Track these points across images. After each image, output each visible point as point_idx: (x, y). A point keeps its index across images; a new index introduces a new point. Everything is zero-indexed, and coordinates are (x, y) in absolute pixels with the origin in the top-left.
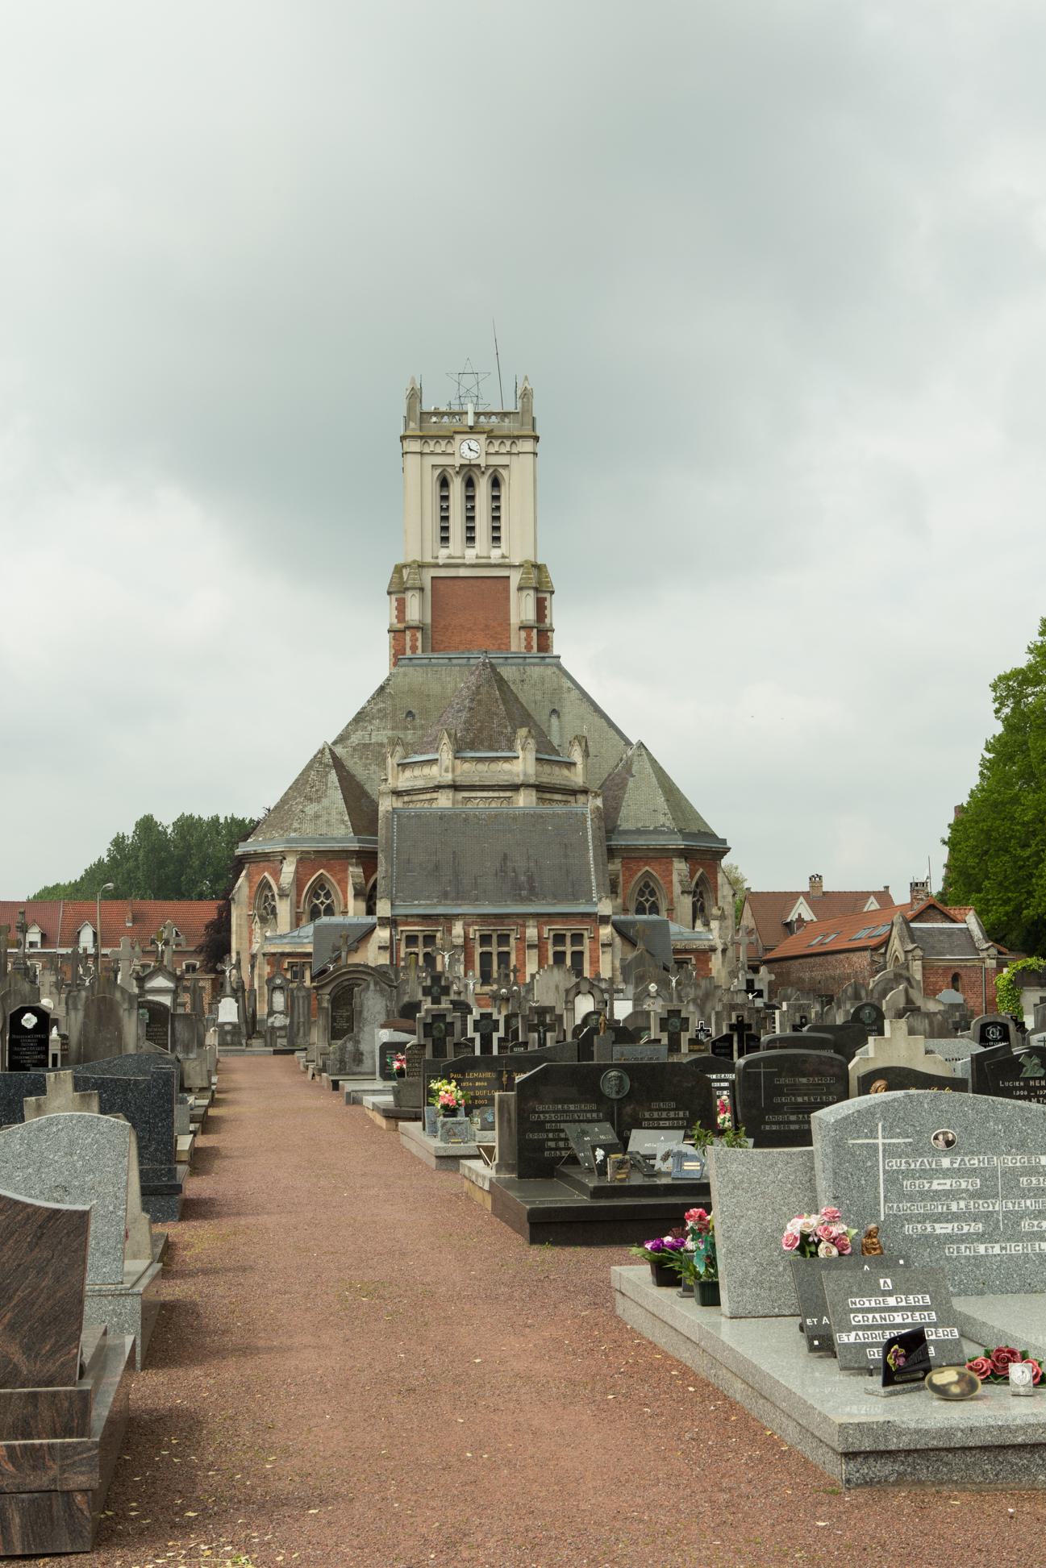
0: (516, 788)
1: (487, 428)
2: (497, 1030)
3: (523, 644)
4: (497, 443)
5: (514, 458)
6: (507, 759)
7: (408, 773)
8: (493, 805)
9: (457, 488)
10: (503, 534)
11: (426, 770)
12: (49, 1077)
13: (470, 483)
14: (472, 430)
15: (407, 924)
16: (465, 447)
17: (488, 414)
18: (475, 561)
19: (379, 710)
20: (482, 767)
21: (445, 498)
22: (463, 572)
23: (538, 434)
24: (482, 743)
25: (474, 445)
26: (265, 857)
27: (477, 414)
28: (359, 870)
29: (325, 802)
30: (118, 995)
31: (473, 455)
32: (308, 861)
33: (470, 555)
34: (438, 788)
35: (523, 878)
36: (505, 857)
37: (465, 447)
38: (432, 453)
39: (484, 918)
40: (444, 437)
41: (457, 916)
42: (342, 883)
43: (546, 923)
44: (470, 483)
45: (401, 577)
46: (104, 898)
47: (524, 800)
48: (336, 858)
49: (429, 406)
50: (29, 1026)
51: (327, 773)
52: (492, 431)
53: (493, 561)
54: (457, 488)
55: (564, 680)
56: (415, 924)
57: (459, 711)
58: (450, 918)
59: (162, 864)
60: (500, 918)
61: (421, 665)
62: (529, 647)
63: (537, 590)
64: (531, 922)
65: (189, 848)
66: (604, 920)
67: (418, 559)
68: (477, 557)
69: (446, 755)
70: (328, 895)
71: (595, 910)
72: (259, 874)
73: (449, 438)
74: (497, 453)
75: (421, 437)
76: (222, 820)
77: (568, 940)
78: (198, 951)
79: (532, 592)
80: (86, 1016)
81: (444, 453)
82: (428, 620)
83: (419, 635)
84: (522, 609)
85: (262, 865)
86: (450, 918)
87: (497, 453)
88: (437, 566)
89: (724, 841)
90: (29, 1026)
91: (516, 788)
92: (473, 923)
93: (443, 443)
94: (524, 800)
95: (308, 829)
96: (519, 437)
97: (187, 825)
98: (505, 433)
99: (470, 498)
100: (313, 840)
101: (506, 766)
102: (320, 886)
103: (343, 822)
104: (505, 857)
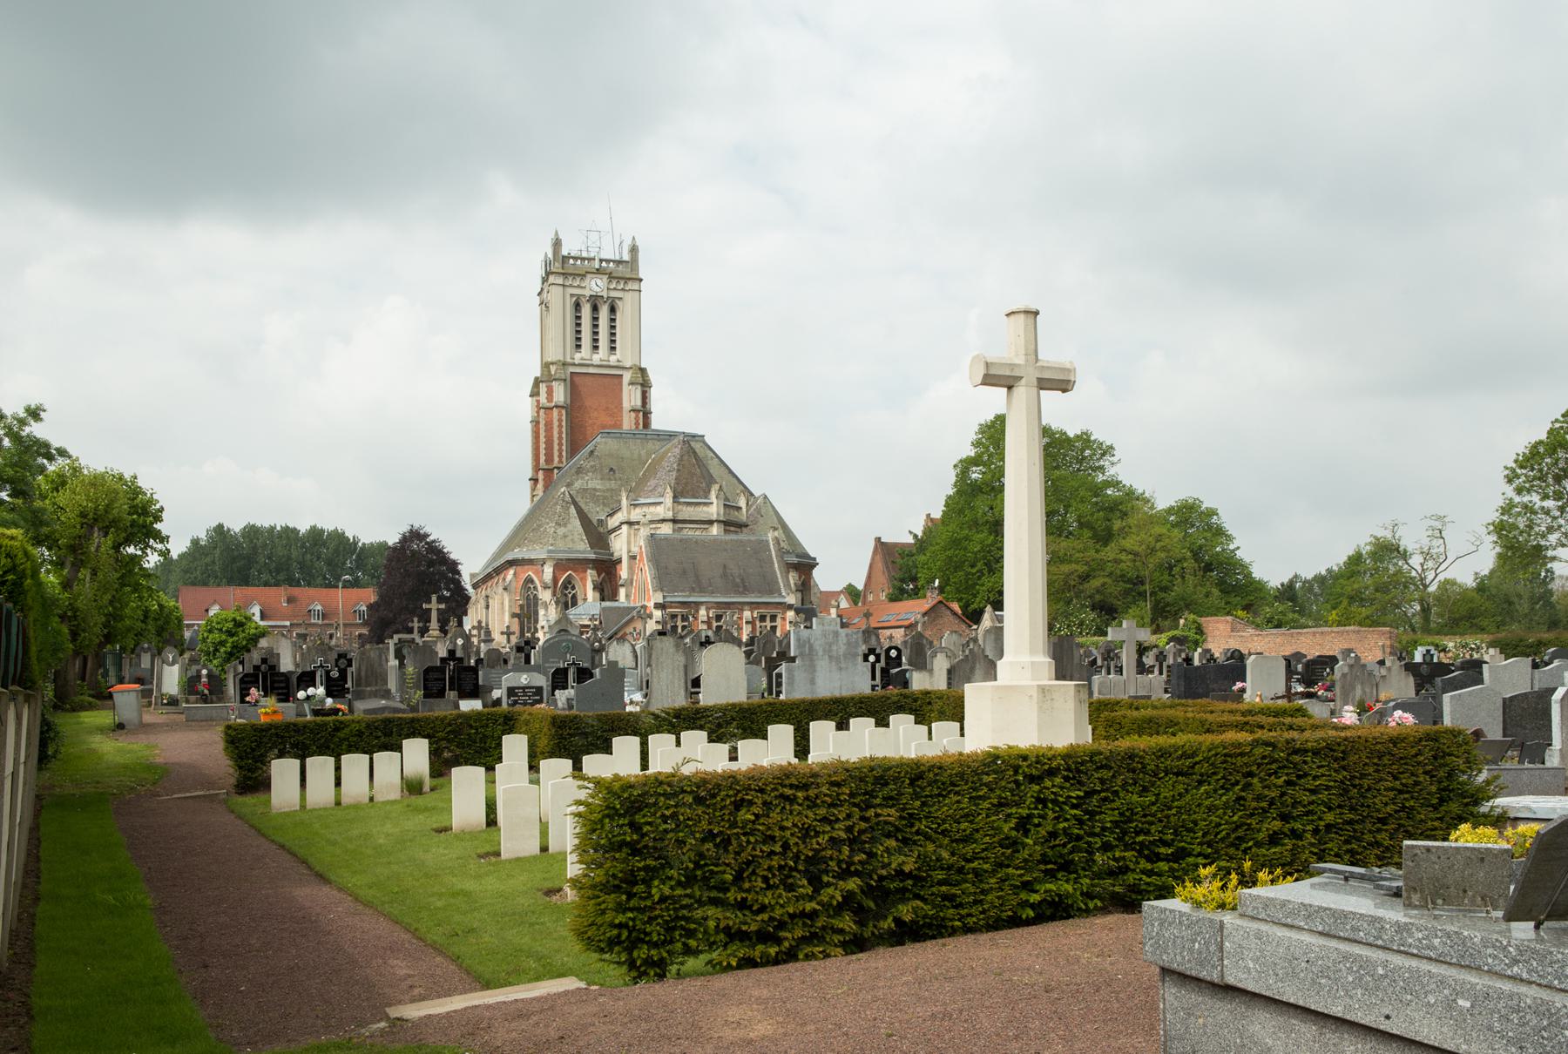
0: (711, 522)
1: (608, 271)
2: (882, 669)
3: (634, 422)
4: (614, 282)
5: (626, 293)
6: (705, 504)
7: (638, 510)
8: (697, 533)
9: (586, 311)
10: (618, 345)
11: (652, 509)
12: (367, 712)
13: (595, 309)
14: (599, 271)
15: (671, 607)
16: (593, 283)
17: (608, 261)
18: (599, 363)
19: (592, 467)
20: (691, 509)
21: (579, 318)
22: (591, 370)
23: (641, 276)
24: (688, 492)
25: (599, 282)
26: (530, 562)
27: (601, 261)
28: (594, 572)
29: (570, 527)
30: (925, 641)
31: (598, 289)
32: (560, 566)
33: (596, 358)
34: (663, 521)
35: (738, 580)
36: (725, 566)
37: (593, 283)
38: (571, 286)
39: (719, 605)
40: (579, 275)
41: (702, 603)
42: (584, 580)
43: (756, 609)
44: (595, 309)
45: (549, 371)
46: (344, 587)
47: (715, 530)
48: (580, 564)
49: (565, 252)
50: (894, 656)
51: (569, 508)
52: (611, 273)
53: (611, 364)
54: (586, 311)
55: (708, 452)
56: (676, 608)
57: (670, 471)
58: (698, 605)
59: (234, 560)
60: (728, 605)
61: (616, 438)
62: (637, 424)
63: (642, 385)
64: (746, 607)
65: (255, 548)
66: (790, 607)
67: (562, 359)
68: (601, 360)
69: (668, 499)
70: (573, 588)
71: (786, 600)
72: (525, 573)
73: (583, 276)
74: (615, 289)
75: (563, 274)
76: (279, 528)
77: (768, 619)
78: (365, 624)
79: (639, 387)
80: (911, 651)
81: (579, 286)
82: (569, 402)
83: (564, 412)
84: (631, 397)
85: (526, 567)
86: (698, 605)
87: (615, 289)
88: (574, 365)
89: (815, 559)
90: (894, 656)
91: (711, 522)
92: (712, 608)
93: (578, 279)
94: (715, 530)
95: (561, 545)
96: (630, 279)
97: (252, 532)
98: (620, 275)
99: (596, 319)
100: (565, 552)
101: (705, 509)
102: (568, 583)
103: (582, 540)
104: (725, 566)
